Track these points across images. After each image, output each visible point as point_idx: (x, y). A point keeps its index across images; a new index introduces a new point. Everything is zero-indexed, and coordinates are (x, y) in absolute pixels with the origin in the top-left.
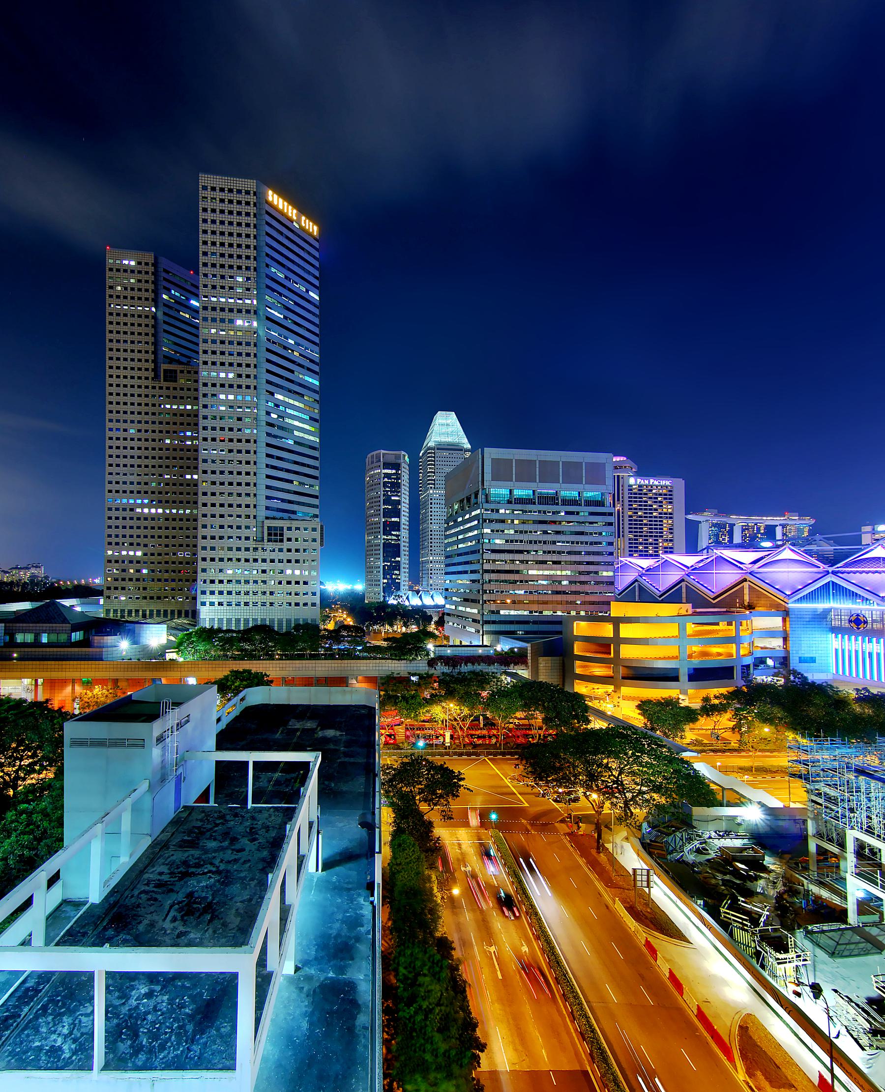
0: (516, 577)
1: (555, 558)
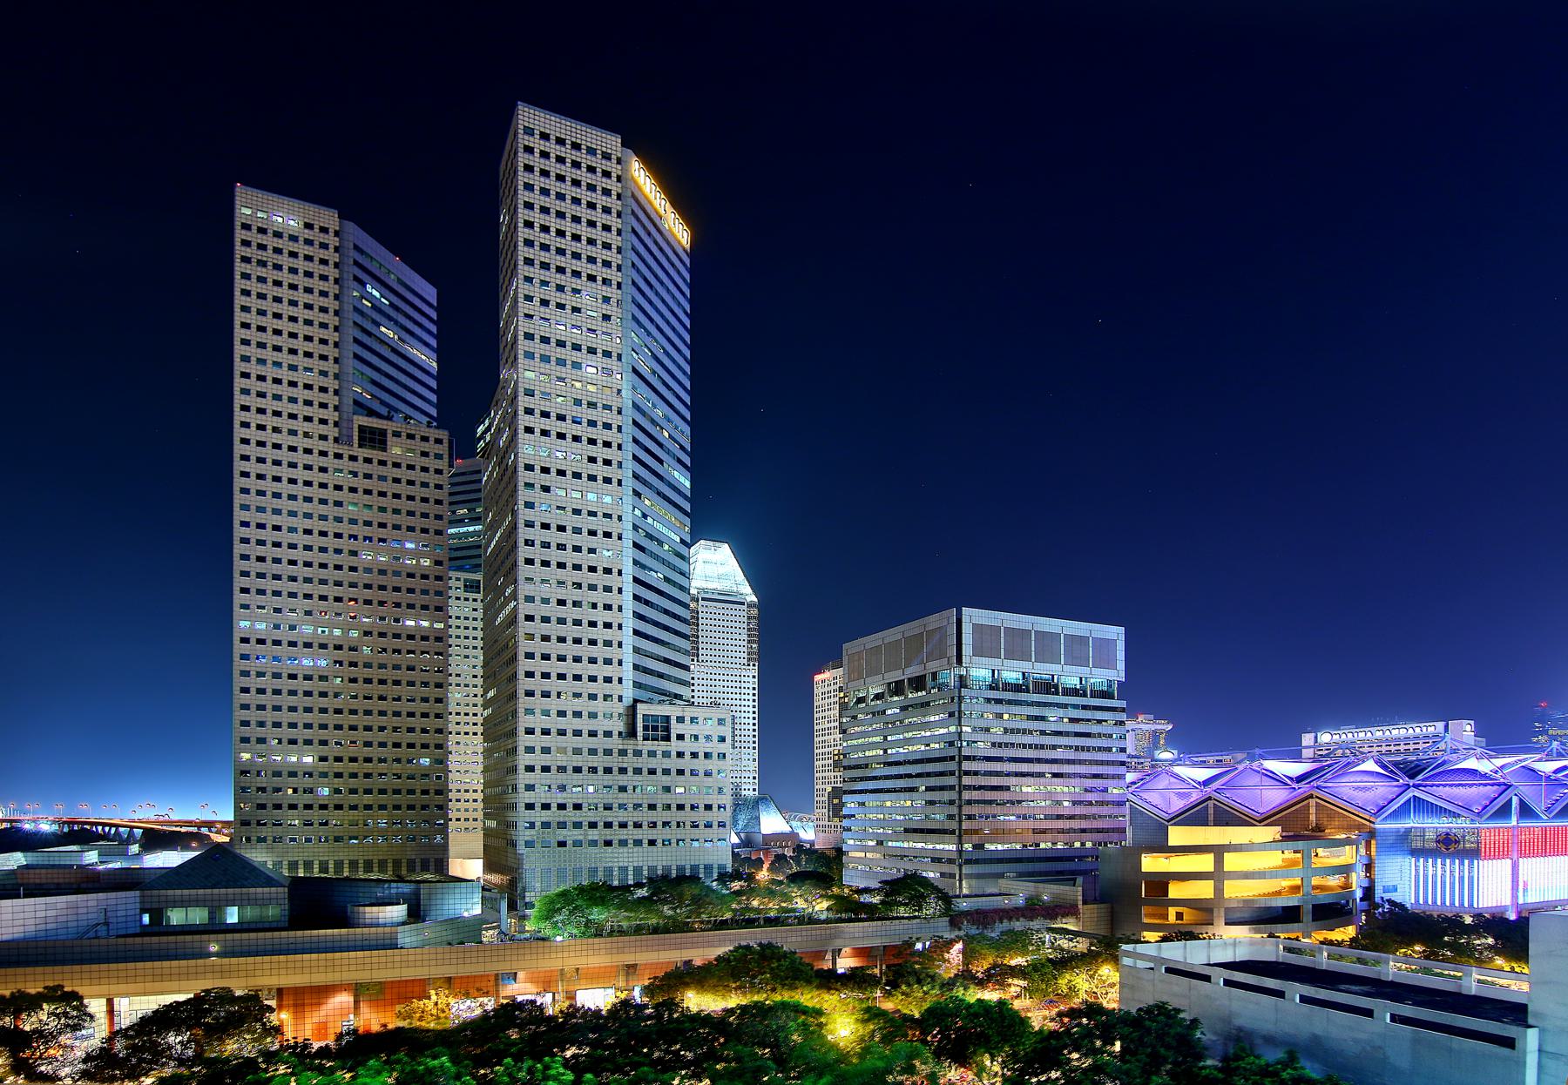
0: (1005, 796)
1: (1056, 768)
